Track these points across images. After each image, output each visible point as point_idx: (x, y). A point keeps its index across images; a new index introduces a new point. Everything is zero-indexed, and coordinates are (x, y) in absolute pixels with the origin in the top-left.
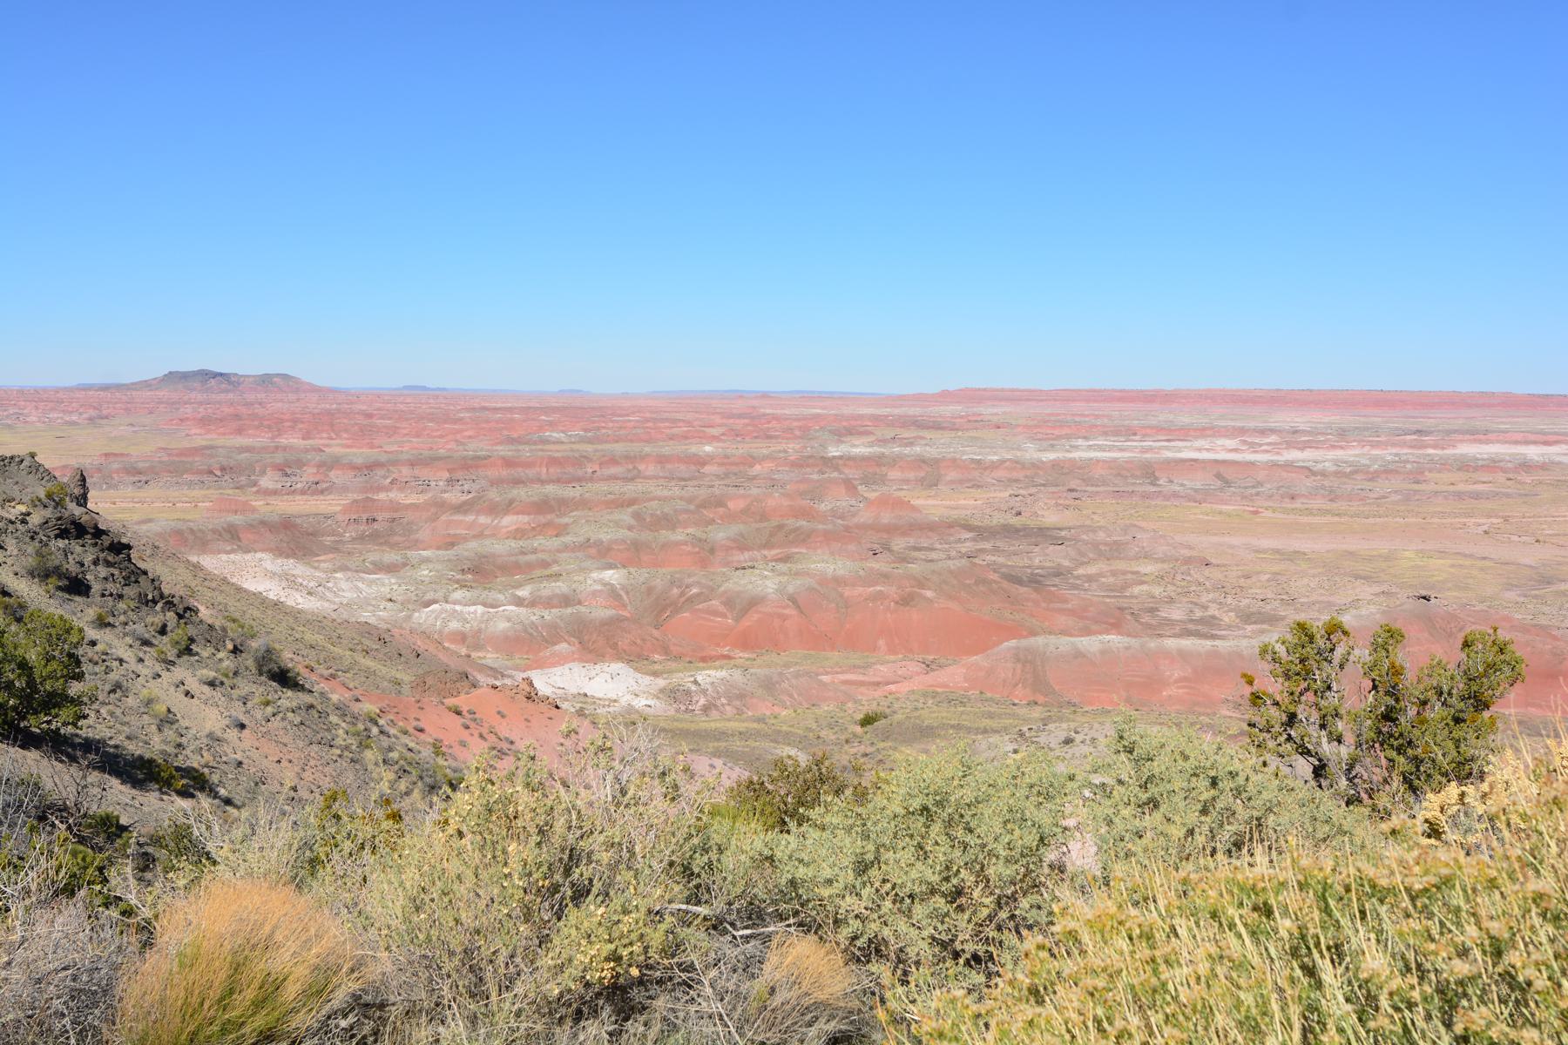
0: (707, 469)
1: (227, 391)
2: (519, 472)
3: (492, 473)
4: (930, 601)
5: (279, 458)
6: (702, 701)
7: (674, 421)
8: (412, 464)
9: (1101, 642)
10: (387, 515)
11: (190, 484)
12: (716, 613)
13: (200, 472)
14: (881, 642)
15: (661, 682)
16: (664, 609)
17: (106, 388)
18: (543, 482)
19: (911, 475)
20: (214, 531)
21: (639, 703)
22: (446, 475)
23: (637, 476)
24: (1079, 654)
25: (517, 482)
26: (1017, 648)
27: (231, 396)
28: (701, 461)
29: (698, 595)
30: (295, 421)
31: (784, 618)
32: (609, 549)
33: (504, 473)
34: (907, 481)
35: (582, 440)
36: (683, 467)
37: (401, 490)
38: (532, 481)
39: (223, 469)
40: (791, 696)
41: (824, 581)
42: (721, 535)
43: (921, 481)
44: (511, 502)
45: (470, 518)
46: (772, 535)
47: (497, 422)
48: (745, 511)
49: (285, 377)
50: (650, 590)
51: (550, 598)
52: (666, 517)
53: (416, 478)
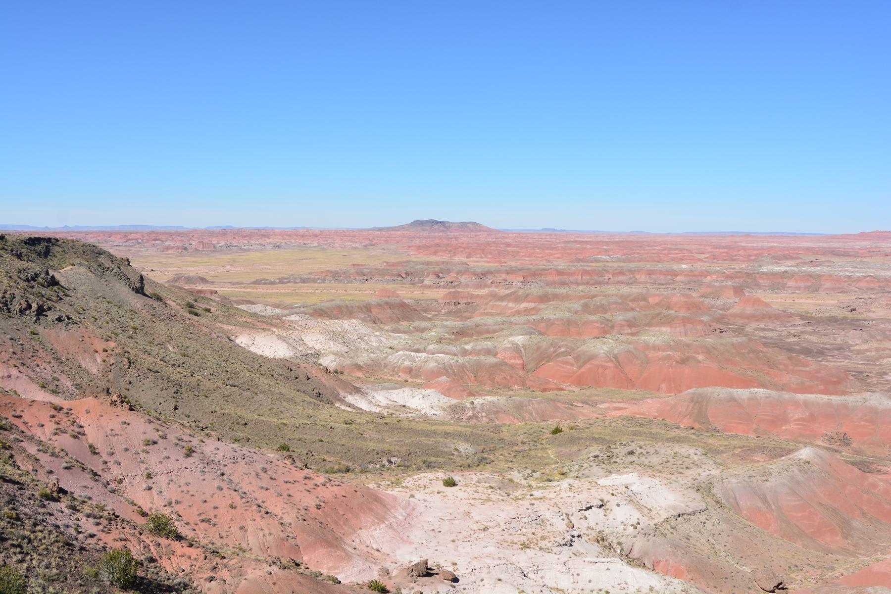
0: (678, 278)
1: (443, 231)
2: (566, 278)
3: (549, 278)
4: (699, 362)
5: (437, 269)
6: (470, 414)
7: (681, 250)
8: (508, 273)
9: (750, 393)
10: (466, 301)
11: (388, 282)
12: (567, 363)
13: (393, 275)
14: (663, 386)
15: (454, 401)
16: (543, 359)
17: (380, 229)
18: (578, 284)
19: (802, 284)
20: (358, 307)
21: (430, 413)
22: (522, 279)
23: (635, 282)
24: (732, 399)
25: (564, 284)
26: (694, 394)
27: (441, 234)
28: (675, 274)
29: (564, 352)
30: (465, 248)
31: (605, 368)
32: (553, 324)
33: (557, 278)
34: (798, 288)
35: (619, 260)
36: (662, 277)
37: (496, 287)
38: (572, 283)
39: (407, 274)
40: (531, 414)
41: (647, 347)
42: (621, 318)
43: (807, 288)
44: (528, 295)
45: (504, 304)
46: (653, 318)
47: (576, 249)
48: (658, 304)
49: (474, 223)
50: (538, 348)
51: (480, 350)
52: (602, 306)
53: (505, 280)
